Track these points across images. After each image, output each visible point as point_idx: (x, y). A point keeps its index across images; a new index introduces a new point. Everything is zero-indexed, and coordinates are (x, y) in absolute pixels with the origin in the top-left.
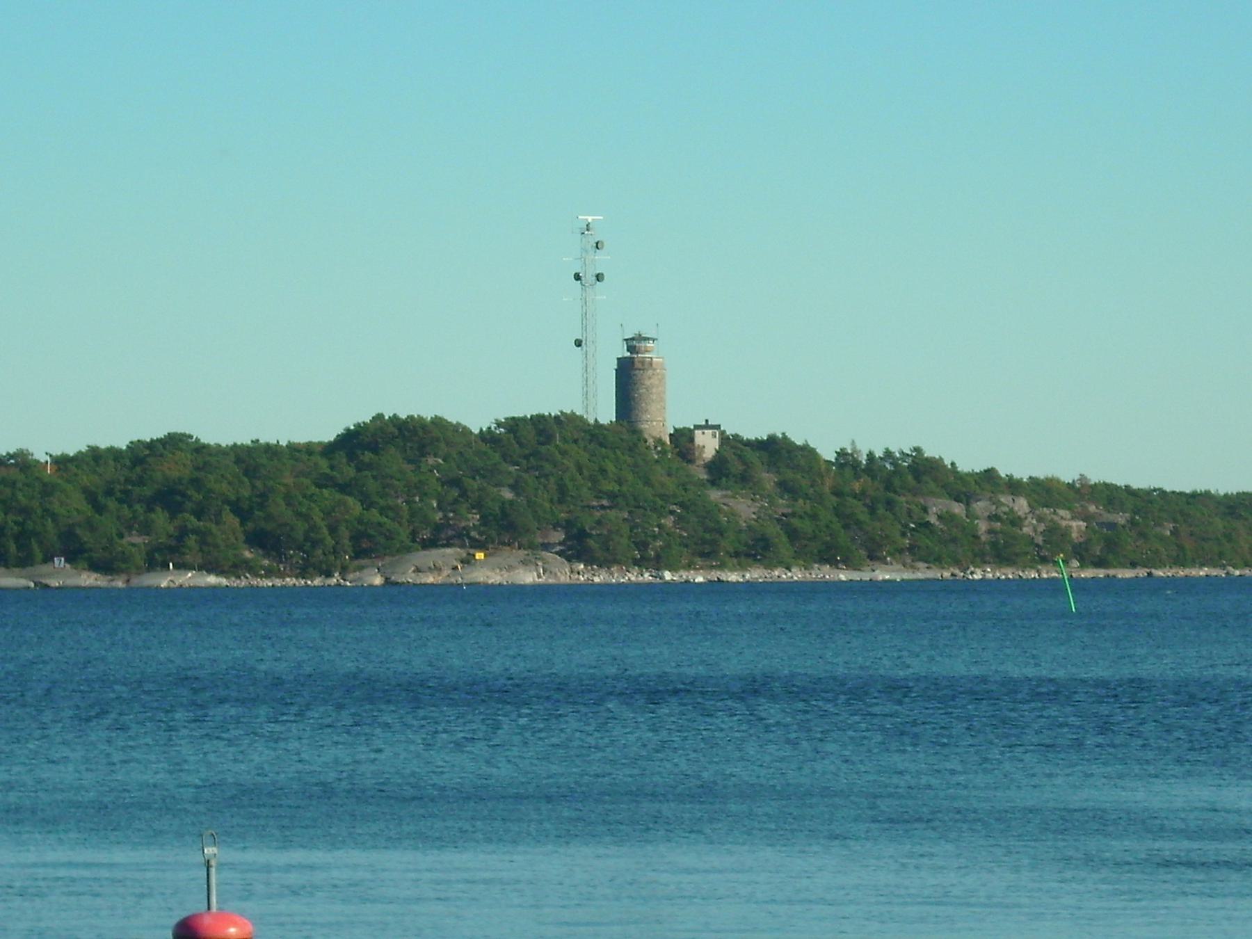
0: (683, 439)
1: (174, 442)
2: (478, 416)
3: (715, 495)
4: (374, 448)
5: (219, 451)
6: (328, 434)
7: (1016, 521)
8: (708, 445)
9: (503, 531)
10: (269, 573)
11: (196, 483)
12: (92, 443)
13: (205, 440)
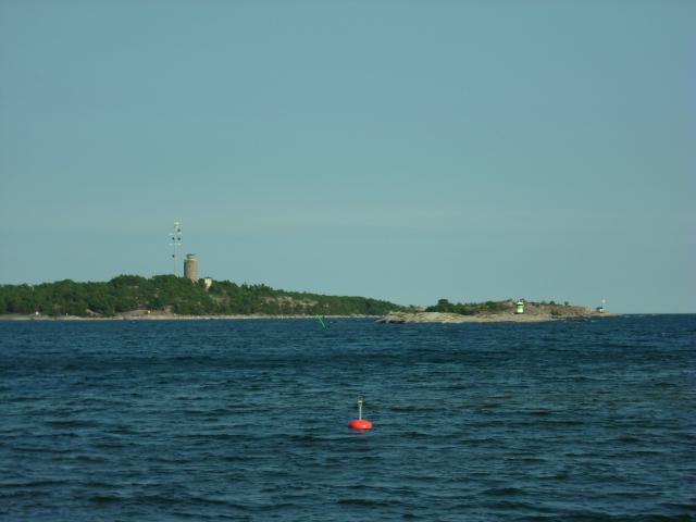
0: (202, 281)
1: (67, 282)
2: (148, 274)
3: (211, 296)
4: (120, 283)
5: (78, 284)
6: (108, 280)
7: (288, 303)
8: (208, 283)
9: (156, 306)
10: (94, 316)
11: (74, 293)
12: (413, 304)
13: (76, 281)
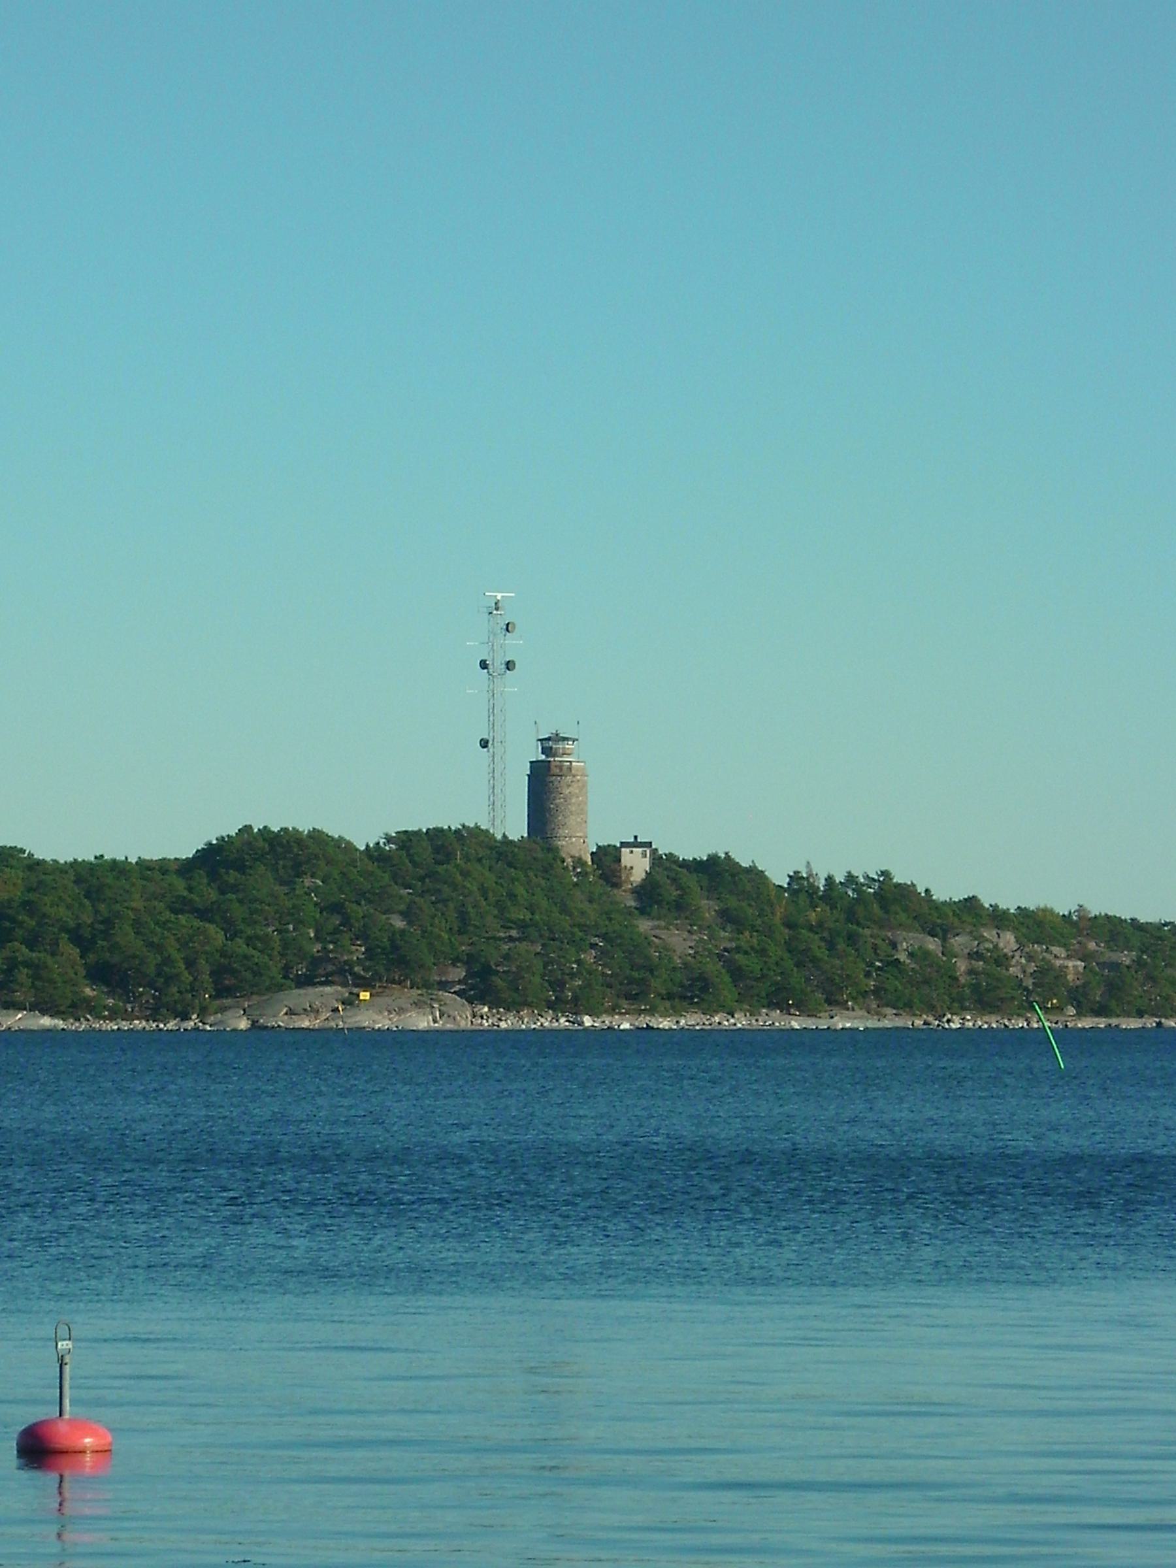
2: (364, 830)
3: (644, 925)
5: (58, 869)
7: (1002, 960)
8: (637, 865)
